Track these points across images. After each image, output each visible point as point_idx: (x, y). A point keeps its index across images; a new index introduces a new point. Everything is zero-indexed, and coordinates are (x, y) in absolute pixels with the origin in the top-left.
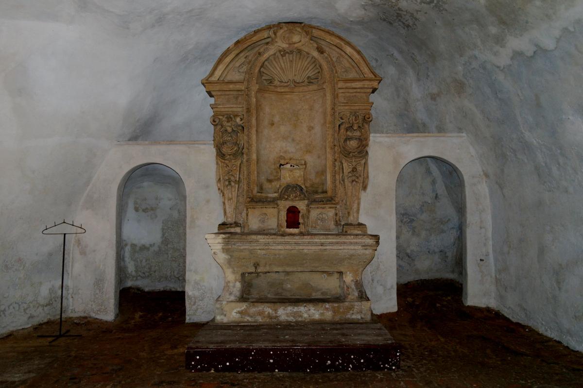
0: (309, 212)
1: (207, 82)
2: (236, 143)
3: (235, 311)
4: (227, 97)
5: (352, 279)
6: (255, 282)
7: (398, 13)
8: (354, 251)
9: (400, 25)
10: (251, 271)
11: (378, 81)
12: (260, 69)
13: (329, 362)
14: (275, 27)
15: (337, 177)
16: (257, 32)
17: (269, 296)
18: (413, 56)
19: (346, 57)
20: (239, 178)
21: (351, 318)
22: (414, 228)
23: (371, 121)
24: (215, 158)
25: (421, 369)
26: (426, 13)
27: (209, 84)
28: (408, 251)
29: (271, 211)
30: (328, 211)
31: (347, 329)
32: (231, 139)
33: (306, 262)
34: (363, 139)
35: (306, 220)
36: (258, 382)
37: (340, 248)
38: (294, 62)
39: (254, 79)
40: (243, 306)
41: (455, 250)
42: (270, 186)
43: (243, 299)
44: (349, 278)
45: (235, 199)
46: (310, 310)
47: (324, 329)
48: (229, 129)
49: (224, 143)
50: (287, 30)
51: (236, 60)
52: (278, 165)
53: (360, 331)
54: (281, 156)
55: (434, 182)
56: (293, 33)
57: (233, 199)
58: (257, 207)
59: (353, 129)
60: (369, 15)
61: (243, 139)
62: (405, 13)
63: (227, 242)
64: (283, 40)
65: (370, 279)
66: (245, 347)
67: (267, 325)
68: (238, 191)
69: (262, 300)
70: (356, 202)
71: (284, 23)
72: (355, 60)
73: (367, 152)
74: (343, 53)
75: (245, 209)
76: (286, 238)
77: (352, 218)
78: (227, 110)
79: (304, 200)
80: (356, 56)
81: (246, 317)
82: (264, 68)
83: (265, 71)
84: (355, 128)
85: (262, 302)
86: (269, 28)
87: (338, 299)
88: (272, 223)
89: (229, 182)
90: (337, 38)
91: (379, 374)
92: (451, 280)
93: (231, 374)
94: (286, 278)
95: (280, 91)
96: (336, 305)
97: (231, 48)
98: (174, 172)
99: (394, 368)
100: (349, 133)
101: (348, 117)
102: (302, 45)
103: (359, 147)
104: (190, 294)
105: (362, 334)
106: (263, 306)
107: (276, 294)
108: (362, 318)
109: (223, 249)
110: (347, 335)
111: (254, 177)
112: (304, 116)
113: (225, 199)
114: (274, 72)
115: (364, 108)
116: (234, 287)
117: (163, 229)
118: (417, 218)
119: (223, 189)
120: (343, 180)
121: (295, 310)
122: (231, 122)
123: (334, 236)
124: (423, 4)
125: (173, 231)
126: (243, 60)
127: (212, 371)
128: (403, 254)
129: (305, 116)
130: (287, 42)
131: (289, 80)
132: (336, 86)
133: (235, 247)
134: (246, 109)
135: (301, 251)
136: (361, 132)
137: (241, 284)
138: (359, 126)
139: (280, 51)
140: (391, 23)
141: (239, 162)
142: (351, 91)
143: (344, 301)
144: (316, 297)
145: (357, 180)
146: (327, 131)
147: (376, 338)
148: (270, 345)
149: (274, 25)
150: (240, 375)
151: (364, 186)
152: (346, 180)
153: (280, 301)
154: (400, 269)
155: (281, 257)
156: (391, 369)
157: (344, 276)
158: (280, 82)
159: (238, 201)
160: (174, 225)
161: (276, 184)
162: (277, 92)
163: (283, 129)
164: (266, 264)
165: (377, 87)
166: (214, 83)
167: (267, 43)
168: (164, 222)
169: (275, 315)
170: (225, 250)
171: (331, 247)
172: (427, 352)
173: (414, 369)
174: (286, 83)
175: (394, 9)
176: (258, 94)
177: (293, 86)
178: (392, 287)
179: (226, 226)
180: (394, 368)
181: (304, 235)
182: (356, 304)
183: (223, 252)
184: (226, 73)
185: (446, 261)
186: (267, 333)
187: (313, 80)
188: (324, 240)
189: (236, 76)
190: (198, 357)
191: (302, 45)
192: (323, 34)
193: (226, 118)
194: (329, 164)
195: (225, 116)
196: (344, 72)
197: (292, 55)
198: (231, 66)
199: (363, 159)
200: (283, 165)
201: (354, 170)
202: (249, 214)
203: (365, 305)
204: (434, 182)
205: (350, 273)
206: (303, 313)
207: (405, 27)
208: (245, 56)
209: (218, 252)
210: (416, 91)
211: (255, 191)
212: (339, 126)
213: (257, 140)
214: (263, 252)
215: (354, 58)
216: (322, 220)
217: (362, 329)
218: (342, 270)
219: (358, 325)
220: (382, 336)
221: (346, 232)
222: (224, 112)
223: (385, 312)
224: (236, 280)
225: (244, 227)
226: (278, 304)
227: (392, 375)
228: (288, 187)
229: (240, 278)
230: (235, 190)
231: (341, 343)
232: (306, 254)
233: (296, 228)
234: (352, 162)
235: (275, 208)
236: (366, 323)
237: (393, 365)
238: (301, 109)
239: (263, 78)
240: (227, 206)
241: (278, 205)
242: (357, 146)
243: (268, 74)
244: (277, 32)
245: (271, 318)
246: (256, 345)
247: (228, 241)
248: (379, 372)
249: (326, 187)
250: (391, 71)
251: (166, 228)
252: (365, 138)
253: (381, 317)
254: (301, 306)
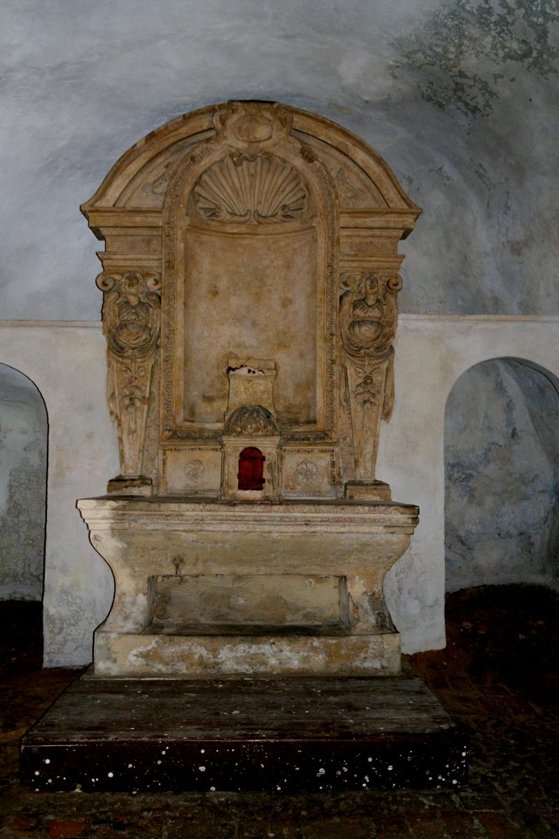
0: (282, 458)
1: (93, 209)
2: (146, 326)
3: (135, 652)
4: (129, 239)
5: (364, 589)
6: (177, 592)
7: (457, 84)
8: (370, 536)
9: (459, 109)
10: (168, 573)
11: (415, 216)
12: (194, 188)
13: (322, 771)
15: (336, 392)
16: (189, 117)
17: (203, 620)
18: (481, 170)
19: (356, 169)
20: (151, 393)
21: (362, 667)
22: (472, 490)
23: (399, 290)
24: (105, 355)
25: (509, 783)
26: (513, 80)
27: (96, 214)
28: (462, 533)
29: (210, 456)
30: (318, 458)
31: (357, 692)
32: (135, 318)
33: (276, 558)
34: (385, 323)
35: (276, 474)
36: (173, 818)
37: (343, 529)
38: (258, 178)
39: (181, 206)
40: (151, 643)
41: (548, 532)
42: (209, 409)
43: (152, 627)
44: (357, 588)
45: (141, 433)
46: (282, 651)
47: (310, 693)
48: (134, 301)
49: (123, 326)
50: (245, 116)
51: (150, 169)
52: (225, 370)
53: (381, 698)
54: (231, 353)
55: (509, 407)
56: (257, 122)
57: (139, 432)
58: (184, 447)
59: (366, 304)
60: (400, 90)
61: (157, 318)
62: (471, 82)
63: (119, 516)
64: (237, 135)
65: (396, 588)
66: (147, 739)
67: (198, 681)
68: (148, 416)
69: (188, 631)
70: (371, 440)
71: (241, 101)
72: (371, 176)
73: (392, 348)
74: (350, 163)
75: (161, 452)
76: (237, 508)
77: (362, 472)
78: (128, 263)
79: (273, 435)
80: (374, 168)
81: (155, 665)
82: (201, 186)
83: (203, 193)
84: (370, 303)
85: (187, 636)
86: (212, 110)
87: (336, 629)
88: (211, 480)
89: (131, 399)
90: (340, 133)
91: (426, 796)
92: (540, 586)
93: (118, 796)
94: (236, 586)
95: (231, 231)
96: (334, 642)
97: (138, 146)
98: (14, 371)
99: (455, 782)
100: (358, 312)
101: (358, 283)
102: (274, 145)
103: (378, 338)
104: (51, 613)
105: (388, 705)
106: (190, 644)
107: (216, 618)
108: (383, 667)
109: (112, 529)
110: (357, 709)
111: (179, 390)
112: (274, 278)
113: (122, 433)
114: (221, 196)
115: (387, 265)
116: (134, 604)
117: (10, 487)
118: (478, 473)
119: (118, 412)
120: (347, 400)
121: (252, 651)
122: (136, 287)
123: (331, 507)
124: (508, 60)
125: (30, 490)
126: (162, 170)
127: (78, 790)
128: (456, 540)
129: (277, 278)
130: (245, 138)
131: (248, 210)
132: (335, 222)
133: (137, 525)
134: (166, 262)
135: (266, 535)
136: (381, 310)
137: (149, 599)
138: (378, 300)
139: (232, 155)
140: (441, 106)
141: (150, 363)
142: (363, 233)
143: (347, 632)
144: (293, 623)
145: (372, 400)
146: (317, 307)
147: (415, 715)
148: (199, 733)
149: (222, 105)
150: (136, 800)
151: (386, 411)
152: (352, 400)
153: (223, 632)
154: (451, 568)
155: (227, 546)
156: (447, 784)
157: (349, 584)
158: (232, 214)
159: (147, 437)
160: (32, 478)
161: (220, 406)
162: (225, 233)
163: (234, 302)
164: (197, 559)
165: (411, 227)
166: (106, 212)
167: (208, 140)
168: (13, 473)
169: (212, 660)
170: (117, 533)
171: (323, 529)
172: (512, 738)
173: (496, 784)
174: (241, 216)
175: (451, 74)
176: (188, 235)
177: (256, 223)
178: (436, 601)
179: (124, 484)
180: (455, 782)
181: (272, 504)
182: (373, 639)
183: (113, 535)
184: (128, 195)
185: (530, 552)
186: (195, 702)
187: (295, 212)
188: (312, 515)
189: (149, 202)
190: (48, 761)
191: (274, 145)
192: (312, 124)
193: (127, 277)
194: (321, 369)
195: (126, 275)
196: (351, 198)
197: (253, 163)
198: (138, 181)
199: (384, 361)
200: (234, 370)
201: (368, 380)
202: (168, 461)
203: (390, 642)
204: (509, 407)
205: (360, 579)
206: (268, 658)
207: (469, 112)
208: (165, 163)
209: (102, 535)
210: (483, 238)
211: (180, 419)
212: (341, 298)
213: (186, 322)
214: (193, 536)
215: (370, 173)
216: (308, 474)
217: (386, 693)
218: (346, 573)
219: (376, 683)
220: (425, 711)
221: (351, 497)
222: (124, 268)
223: (423, 650)
224: (137, 591)
225: (158, 486)
226: (220, 638)
227: (452, 801)
228: (242, 410)
229: (146, 586)
230: (142, 416)
231: (345, 730)
232: (276, 542)
233: (257, 489)
234: (364, 365)
235: (216, 450)
236: (392, 677)
237: (454, 776)
238: (269, 266)
239: (200, 205)
240: (126, 448)
241: (223, 446)
242: (373, 336)
243: (210, 199)
244: (227, 118)
245: (205, 667)
246: (171, 736)
247: (124, 515)
248: (425, 792)
249: (315, 412)
250: (434, 200)
251: (16, 484)
252: (388, 322)
253: (412, 661)
254: (265, 642)
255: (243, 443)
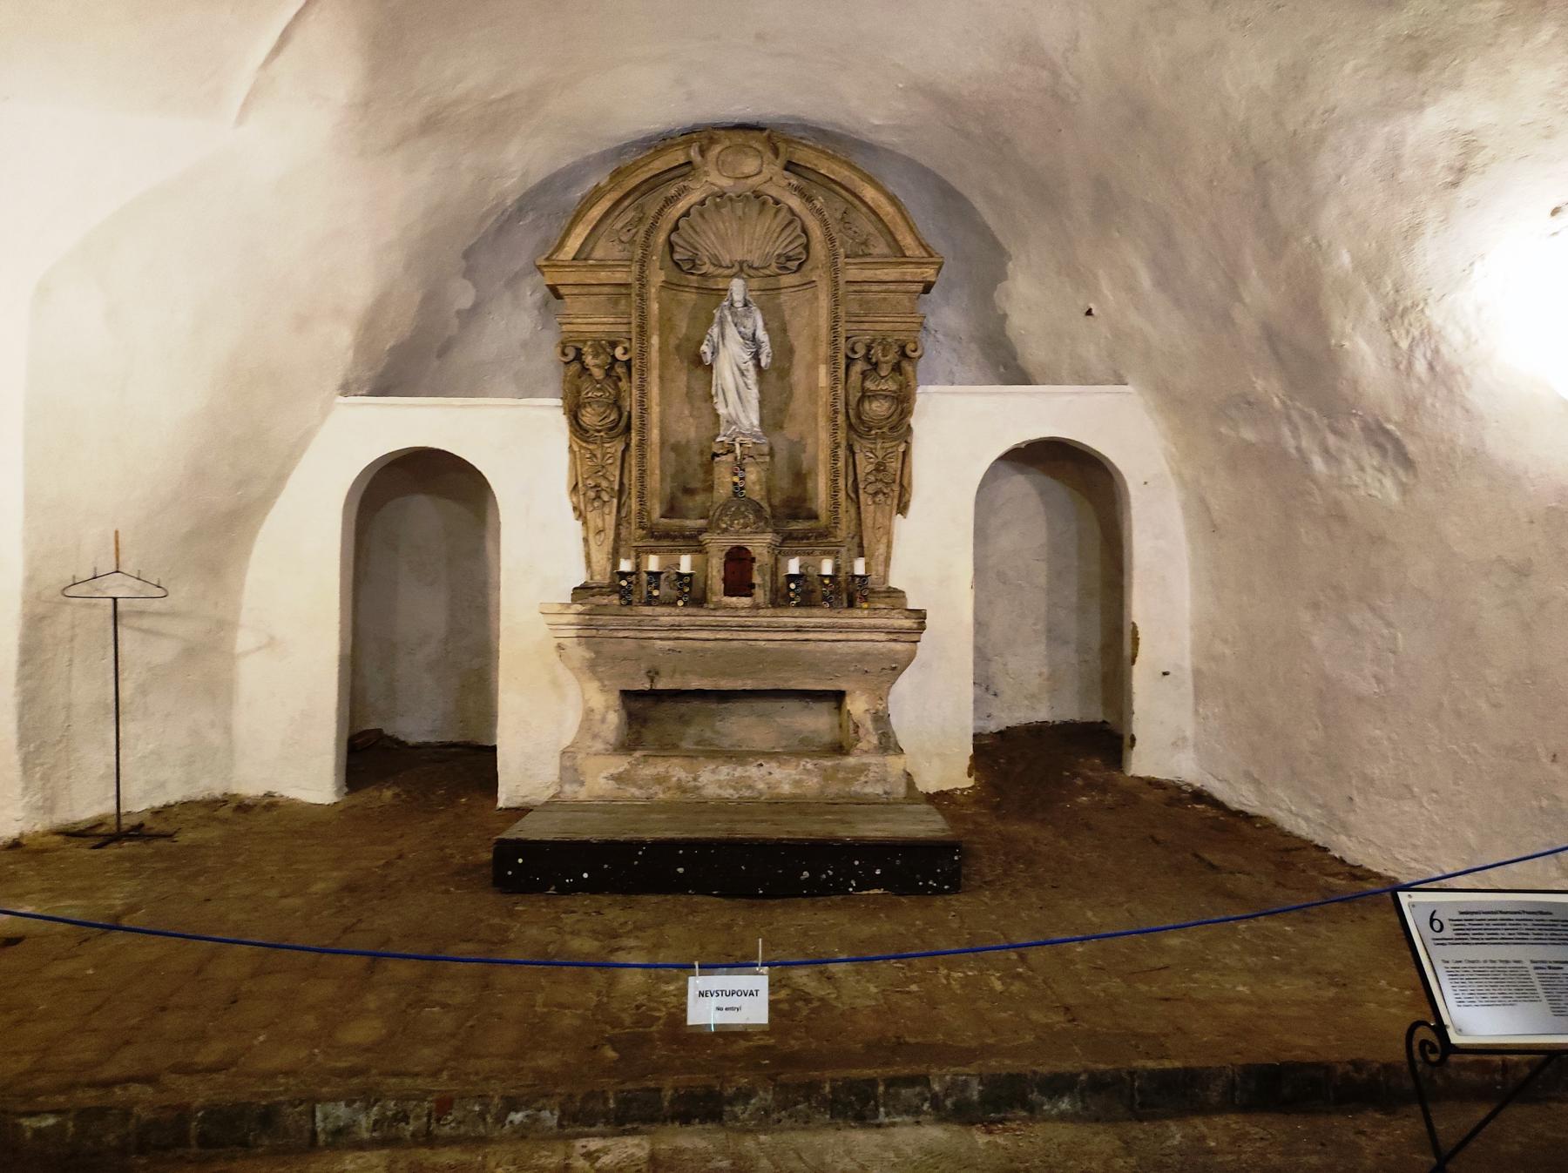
4: (592, 298)
5: (866, 707)
13: (806, 874)
14: (703, 135)
19: (864, 209)
40: (621, 764)
70: (884, 540)
73: (909, 427)
74: (857, 202)
78: (593, 328)
107: (698, 743)
115: (903, 327)
116: (603, 720)
126: (631, 214)
201: (880, 468)
218: (843, 686)
224: (607, 708)
255: (729, 541)
